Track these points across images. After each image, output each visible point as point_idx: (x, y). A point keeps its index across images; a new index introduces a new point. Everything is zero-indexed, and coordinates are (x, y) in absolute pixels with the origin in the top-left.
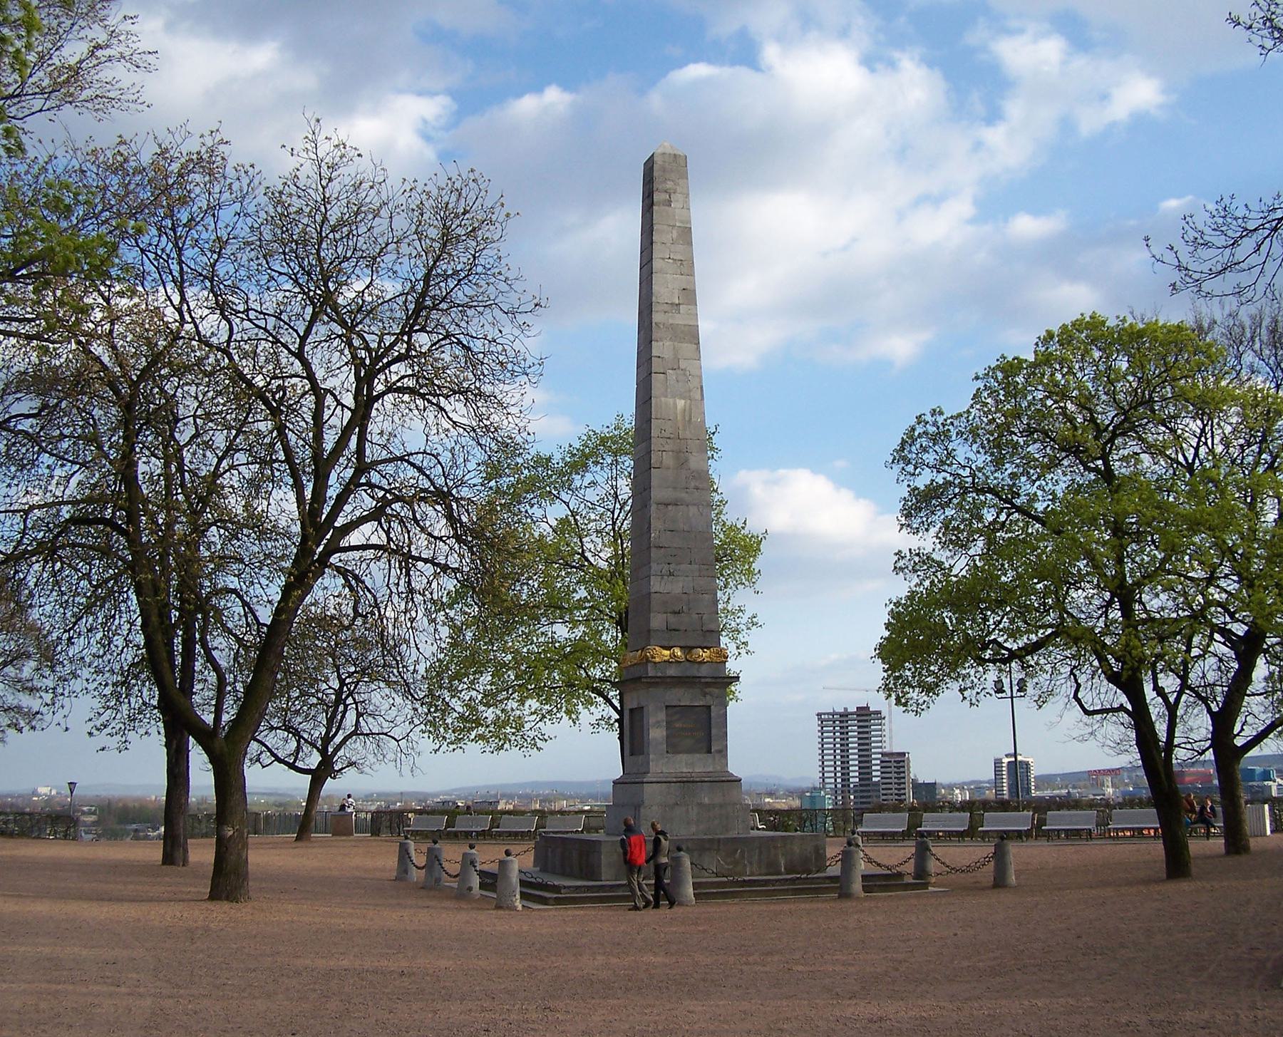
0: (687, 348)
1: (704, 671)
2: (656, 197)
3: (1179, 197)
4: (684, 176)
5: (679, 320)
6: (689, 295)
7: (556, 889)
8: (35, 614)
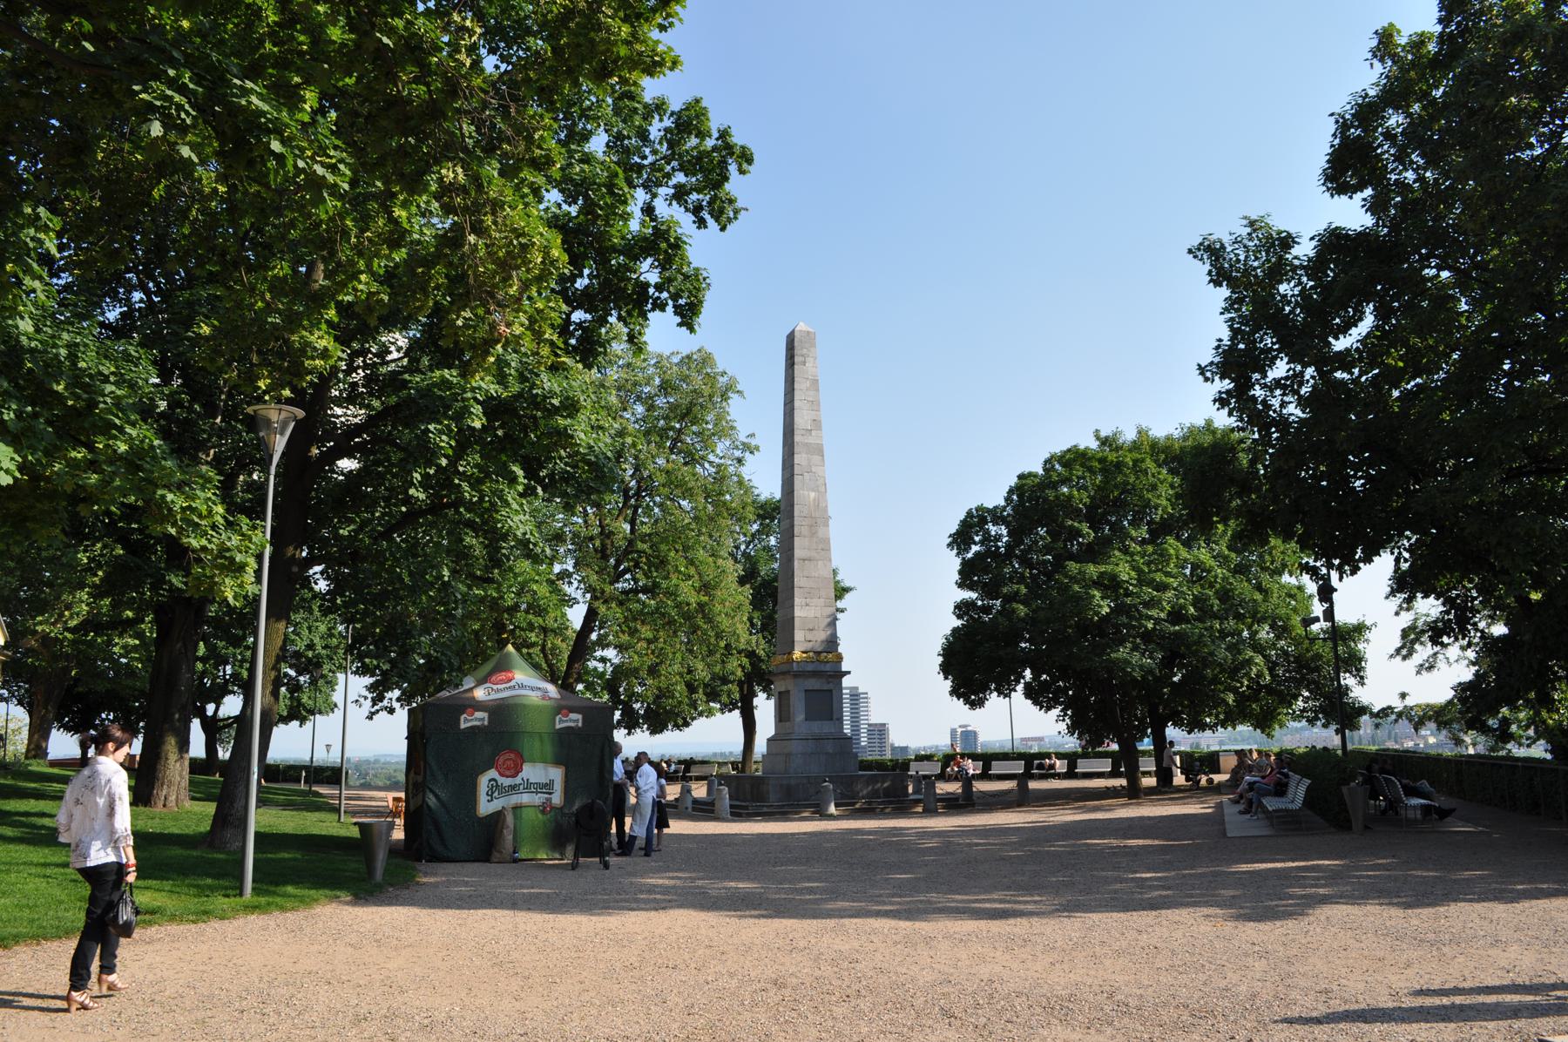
0: (816, 458)
1: (828, 668)
2: (797, 359)
3: (1510, 757)
4: (814, 345)
5: (811, 440)
6: (817, 423)
7: (746, 808)
8: (1267, 628)
